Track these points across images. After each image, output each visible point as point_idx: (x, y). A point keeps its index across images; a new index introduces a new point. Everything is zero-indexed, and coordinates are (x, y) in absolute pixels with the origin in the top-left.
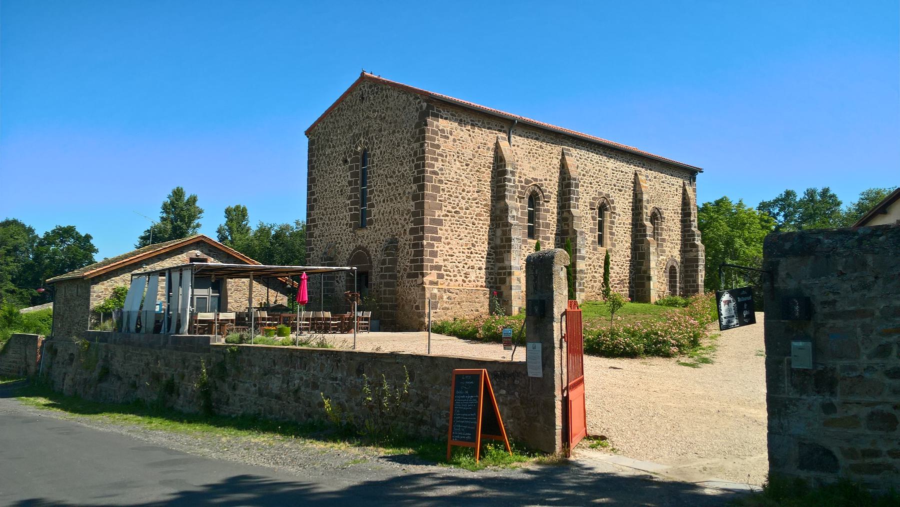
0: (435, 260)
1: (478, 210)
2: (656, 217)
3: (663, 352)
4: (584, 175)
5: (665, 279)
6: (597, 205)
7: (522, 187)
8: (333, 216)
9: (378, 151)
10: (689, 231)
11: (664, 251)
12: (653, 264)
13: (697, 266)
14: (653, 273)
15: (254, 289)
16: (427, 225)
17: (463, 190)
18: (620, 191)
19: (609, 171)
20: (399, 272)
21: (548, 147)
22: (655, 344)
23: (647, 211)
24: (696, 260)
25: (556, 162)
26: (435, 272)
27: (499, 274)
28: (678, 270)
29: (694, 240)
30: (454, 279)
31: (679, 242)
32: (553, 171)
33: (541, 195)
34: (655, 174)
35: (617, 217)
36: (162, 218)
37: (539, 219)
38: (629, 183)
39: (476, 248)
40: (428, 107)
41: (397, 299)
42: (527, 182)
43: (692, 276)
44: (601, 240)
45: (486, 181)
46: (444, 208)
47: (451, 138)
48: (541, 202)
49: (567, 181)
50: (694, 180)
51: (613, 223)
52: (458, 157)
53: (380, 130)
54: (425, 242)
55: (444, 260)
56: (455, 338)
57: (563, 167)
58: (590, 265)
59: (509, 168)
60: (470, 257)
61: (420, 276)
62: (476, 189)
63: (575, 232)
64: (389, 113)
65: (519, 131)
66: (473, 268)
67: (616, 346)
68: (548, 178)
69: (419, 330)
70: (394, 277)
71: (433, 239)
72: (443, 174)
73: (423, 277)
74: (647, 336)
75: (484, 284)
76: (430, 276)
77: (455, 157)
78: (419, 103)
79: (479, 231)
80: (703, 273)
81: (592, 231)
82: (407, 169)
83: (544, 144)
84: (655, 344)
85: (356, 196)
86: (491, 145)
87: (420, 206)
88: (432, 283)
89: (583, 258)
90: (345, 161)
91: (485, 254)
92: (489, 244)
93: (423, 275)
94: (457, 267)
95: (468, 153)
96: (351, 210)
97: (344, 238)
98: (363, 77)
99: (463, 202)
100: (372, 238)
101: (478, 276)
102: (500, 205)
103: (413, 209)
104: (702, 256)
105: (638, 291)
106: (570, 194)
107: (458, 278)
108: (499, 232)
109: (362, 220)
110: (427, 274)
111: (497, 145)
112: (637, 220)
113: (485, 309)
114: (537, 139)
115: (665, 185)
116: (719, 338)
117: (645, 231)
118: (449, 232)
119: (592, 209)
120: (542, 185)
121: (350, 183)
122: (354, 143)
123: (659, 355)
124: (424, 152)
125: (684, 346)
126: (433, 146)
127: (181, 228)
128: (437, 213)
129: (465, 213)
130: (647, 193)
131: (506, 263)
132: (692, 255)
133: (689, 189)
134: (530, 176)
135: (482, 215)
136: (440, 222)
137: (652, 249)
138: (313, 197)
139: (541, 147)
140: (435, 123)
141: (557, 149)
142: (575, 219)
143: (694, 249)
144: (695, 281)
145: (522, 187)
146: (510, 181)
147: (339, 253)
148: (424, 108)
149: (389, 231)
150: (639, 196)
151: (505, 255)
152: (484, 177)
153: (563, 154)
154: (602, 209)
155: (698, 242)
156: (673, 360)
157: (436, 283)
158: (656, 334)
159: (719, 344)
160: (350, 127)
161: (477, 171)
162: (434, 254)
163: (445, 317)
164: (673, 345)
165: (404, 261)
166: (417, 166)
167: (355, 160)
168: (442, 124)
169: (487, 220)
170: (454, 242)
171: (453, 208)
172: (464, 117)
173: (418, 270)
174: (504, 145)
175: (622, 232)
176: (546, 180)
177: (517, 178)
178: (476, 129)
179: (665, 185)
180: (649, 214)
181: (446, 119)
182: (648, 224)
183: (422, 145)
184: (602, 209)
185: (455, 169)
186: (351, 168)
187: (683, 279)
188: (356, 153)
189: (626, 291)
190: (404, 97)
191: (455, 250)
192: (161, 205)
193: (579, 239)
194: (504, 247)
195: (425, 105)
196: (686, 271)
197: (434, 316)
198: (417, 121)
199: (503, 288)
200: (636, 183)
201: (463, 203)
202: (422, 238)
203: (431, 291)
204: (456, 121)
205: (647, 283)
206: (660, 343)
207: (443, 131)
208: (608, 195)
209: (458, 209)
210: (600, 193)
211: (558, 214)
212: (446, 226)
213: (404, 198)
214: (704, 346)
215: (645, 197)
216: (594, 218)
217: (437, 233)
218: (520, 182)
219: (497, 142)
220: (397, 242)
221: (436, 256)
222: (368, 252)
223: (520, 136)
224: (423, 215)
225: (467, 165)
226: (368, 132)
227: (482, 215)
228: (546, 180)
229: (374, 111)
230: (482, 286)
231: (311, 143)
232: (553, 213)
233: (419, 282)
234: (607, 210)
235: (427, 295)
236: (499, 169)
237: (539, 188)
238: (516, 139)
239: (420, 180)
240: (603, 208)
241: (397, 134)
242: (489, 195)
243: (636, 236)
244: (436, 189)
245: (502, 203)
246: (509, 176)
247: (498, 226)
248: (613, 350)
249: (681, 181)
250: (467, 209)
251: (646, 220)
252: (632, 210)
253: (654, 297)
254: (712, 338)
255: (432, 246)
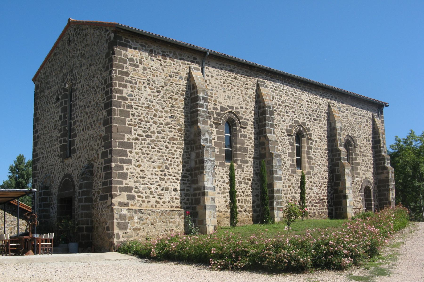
0: (125, 181)
1: (171, 135)
2: (349, 143)
3: (335, 265)
4: (280, 105)
5: (361, 198)
6: (294, 132)
7: (218, 114)
8: (49, 150)
9: (79, 85)
10: (380, 156)
11: (359, 174)
12: (348, 184)
13: (388, 186)
14: (349, 192)
15: (7, 220)
16: (116, 148)
17: (155, 116)
18: (316, 120)
19: (304, 103)
20: (94, 195)
21: (242, 79)
22: (326, 256)
23: (342, 137)
24: (387, 181)
25: (252, 92)
26: (124, 194)
27: (195, 195)
28: (372, 190)
29: (384, 163)
30: (146, 200)
31: (372, 166)
32: (249, 100)
33: (237, 121)
34: (346, 106)
35: (314, 143)
36: (10, 176)
37: (236, 143)
38: (323, 114)
39: (170, 171)
40: (116, 37)
41: (92, 222)
42: (222, 109)
43: (385, 195)
44: (299, 164)
45: (179, 107)
46: (134, 132)
47: (141, 66)
48: (238, 128)
49: (262, 109)
50: (382, 113)
51: (310, 148)
52: (148, 86)
53: (81, 66)
54: (113, 165)
55: (135, 182)
56: (134, 258)
57: (259, 97)
58: (289, 186)
59: (201, 95)
60: (163, 179)
61: (109, 198)
62: (169, 115)
63: (271, 154)
64: (88, 49)
65: (213, 63)
66: (167, 189)
67: (279, 260)
68: (244, 106)
69: (109, 251)
70: (90, 200)
71: (122, 161)
72: (132, 100)
73: (112, 198)
74: (318, 246)
75: (179, 205)
76: (119, 198)
77: (146, 84)
78: (108, 35)
79: (172, 154)
80: (394, 192)
81: (290, 155)
82: (99, 97)
83: (239, 76)
84: (326, 256)
85: (64, 128)
86: (184, 75)
87: (109, 130)
88: (121, 204)
89: (280, 179)
90: (58, 99)
91: (179, 176)
92: (184, 166)
93: (112, 197)
94: (150, 188)
95: (160, 81)
96: (61, 142)
97: (56, 168)
98: (70, 23)
99: (155, 126)
100: (75, 165)
101: (173, 197)
102: (193, 130)
103: (104, 134)
104: (392, 177)
105: (336, 209)
106: (265, 120)
107: (151, 199)
108: (193, 155)
109: (68, 151)
110: (116, 196)
111: (190, 75)
112: (333, 146)
113: (180, 229)
114: (231, 71)
115: (356, 116)
116: (401, 246)
117: (339, 155)
118: (140, 154)
119: (289, 135)
120: (238, 113)
121: (60, 117)
122: (64, 80)
123: (329, 269)
124: (111, 79)
125: (359, 256)
126: (121, 73)
127: (22, 183)
128: (126, 136)
129: (158, 137)
130: (340, 122)
131: (200, 184)
132: (383, 176)
133: (378, 121)
134: (226, 103)
135: (176, 139)
136: (130, 146)
137: (347, 171)
138: (37, 134)
139: (235, 78)
140: (123, 52)
141: (252, 81)
142: (271, 143)
143: (385, 171)
144: (387, 199)
145: (218, 114)
146: (202, 106)
147: (53, 182)
148: (112, 38)
149: (87, 157)
150: (333, 125)
151: (199, 176)
152: (176, 104)
153: (258, 85)
154: (299, 136)
155: (388, 165)
156: (345, 273)
157: (127, 205)
158: (327, 244)
159: (401, 252)
160: (62, 68)
161: (170, 98)
162: (124, 176)
163: (136, 237)
164: (346, 256)
165: (97, 186)
166: (107, 93)
167: (65, 96)
168: (131, 53)
169: (181, 144)
170: (145, 165)
171: (144, 132)
172: (154, 47)
173: (108, 193)
174: (197, 74)
175: (319, 157)
176: (242, 108)
177: (211, 106)
178: (168, 60)
179: (356, 116)
180: (343, 140)
181: (135, 49)
182: (342, 149)
183: (110, 73)
184: (299, 136)
185: (145, 95)
186: (61, 104)
187: (377, 197)
188: (65, 90)
189: (325, 209)
190: (98, 32)
191: (147, 172)
192: (8, 167)
193: (275, 161)
194: (198, 168)
195: (112, 35)
196: (380, 191)
197: (120, 236)
198: (107, 51)
199: (198, 208)
200: (330, 113)
201: (154, 128)
202: (110, 161)
203: (119, 211)
204: (146, 51)
205: (344, 201)
206: (332, 253)
207: (132, 60)
208: (304, 124)
209: (149, 133)
210: (296, 122)
211: (256, 139)
212: (137, 149)
213: (98, 125)
214: (385, 255)
215: (338, 125)
216: (291, 144)
217: (126, 155)
218: (215, 109)
219: (190, 72)
220: (93, 167)
221: (126, 178)
222: (72, 179)
223: (213, 67)
224: (111, 138)
225: (159, 92)
226: (72, 69)
227: (176, 139)
228: (242, 108)
229: (77, 50)
230: (177, 207)
231: (36, 88)
232: (250, 138)
233: (109, 204)
234: (303, 136)
235: (116, 215)
236: (192, 97)
237: (235, 115)
238: (209, 70)
239: (108, 106)
240: (300, 135)
241: (92, 67)
242: (182, 121)
243: (332, 160)
244: (125, 114)
245: (195, 127)
246: (201, 102)
247: (192, 149)
248: (277, 265)
249: (370, 114)
250: (159, 133)
251: (341, 145)
252: (328, 137)
253: (350, 213)
254: (394, 246)
255: (122, 168)
